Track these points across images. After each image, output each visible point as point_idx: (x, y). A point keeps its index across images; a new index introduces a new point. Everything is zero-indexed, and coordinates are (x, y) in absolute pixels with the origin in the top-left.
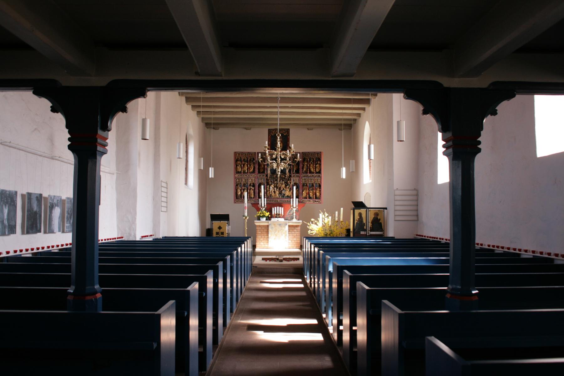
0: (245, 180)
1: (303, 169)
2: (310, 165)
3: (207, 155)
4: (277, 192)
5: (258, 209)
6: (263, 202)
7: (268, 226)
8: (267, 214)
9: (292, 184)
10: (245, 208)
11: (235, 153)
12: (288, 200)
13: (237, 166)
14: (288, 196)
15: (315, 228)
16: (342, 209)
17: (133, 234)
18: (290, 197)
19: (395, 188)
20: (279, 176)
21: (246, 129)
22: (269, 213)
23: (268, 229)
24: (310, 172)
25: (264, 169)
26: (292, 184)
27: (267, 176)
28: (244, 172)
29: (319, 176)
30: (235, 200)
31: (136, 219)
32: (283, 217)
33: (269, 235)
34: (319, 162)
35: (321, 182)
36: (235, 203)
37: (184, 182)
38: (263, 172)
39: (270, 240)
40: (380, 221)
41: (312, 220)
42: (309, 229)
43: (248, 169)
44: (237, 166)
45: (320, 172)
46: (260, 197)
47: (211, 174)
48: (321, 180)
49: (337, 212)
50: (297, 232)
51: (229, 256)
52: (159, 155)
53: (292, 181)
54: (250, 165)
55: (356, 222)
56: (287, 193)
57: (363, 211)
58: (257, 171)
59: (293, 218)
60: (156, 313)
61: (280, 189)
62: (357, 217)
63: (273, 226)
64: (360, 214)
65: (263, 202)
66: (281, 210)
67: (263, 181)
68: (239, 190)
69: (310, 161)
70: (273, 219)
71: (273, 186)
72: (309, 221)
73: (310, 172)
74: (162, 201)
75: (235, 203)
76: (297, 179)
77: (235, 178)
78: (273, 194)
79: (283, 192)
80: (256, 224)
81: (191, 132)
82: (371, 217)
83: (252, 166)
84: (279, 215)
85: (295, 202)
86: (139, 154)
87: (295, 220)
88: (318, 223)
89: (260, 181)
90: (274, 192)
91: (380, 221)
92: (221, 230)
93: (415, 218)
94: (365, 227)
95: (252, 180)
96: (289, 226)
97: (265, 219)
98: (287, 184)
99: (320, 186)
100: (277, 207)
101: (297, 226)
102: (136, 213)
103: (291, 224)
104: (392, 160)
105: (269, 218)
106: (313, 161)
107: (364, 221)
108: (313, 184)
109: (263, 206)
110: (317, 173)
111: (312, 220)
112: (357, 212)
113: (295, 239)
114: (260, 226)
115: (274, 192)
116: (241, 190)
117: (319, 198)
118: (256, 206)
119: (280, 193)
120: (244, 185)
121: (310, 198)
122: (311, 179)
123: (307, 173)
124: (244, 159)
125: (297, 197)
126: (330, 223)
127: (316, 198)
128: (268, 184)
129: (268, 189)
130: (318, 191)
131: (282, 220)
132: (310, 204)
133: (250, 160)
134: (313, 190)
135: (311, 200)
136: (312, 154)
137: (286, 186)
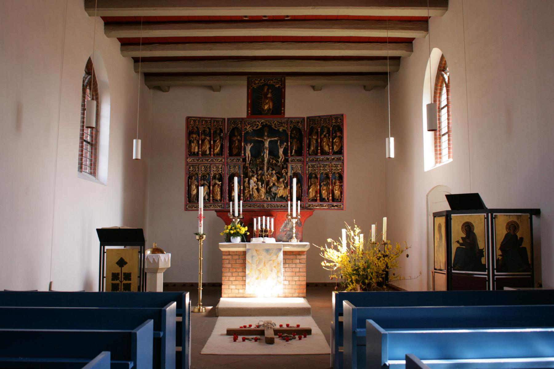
0: (206, 168)
1: (309, 147)
3: (137, 125)
4: (263, 190)
5: (228, 221)
6: (237, 207)
7: (244, 253)
8: (244, 230)
10: (199, 217)
11: (188, 118)
12: (283, 204)
13: (190, 142)
14: (282, 197)
15: (336, 257)
16: (385, 219)
20: (266, 159)
21: (211, 88)
22: (246, 228)
23: (245, 260)
24: (323, 153)
25: (240, 148)
26: (289, 174)
27: (244, 160)
28: (204, 154)
29: (339, 159)
30: (186, 206)
32: (273, 236)
34: (338, 134)
35: (342, 170)
36: (186, 209)
37: (77, 166)
38: (239, 154)
40: (524, 245)
41: (329, 240)
42: (323, 259)
43: (210, 148)
44: (190, 142)
45: (340, 152)
46: (231, 199)
48: (342, 166)
49: (373, 227)
50: (300, 266)
51: (150, 324)
53: (290, 169)
54: (215, 142)
55: (454, 246)
56: (281, 192)
57: (477, 219)
58: (226, 151)
59: (291, 238)
60: (132, 331)
61: (268, 183)
62: (457, 233)
63: (255, 253)
64: (468, 228)
65: (237, 207)
66: (269, 223)
69: (321, 134)
70: (254, 240)
72: (323, 242)
73: (323, 153)
75: (186, 209)
76: (299, 165)
77: (187, 164)
78: (256, 194)
79: (273, 190)
80: (223, 249)
82: (501, 232)
83: (218, 143)
84: (266, 231)
85: (295, 207)
87: (294, 242)
88: (339, 247)
89: (232, 170)
90: (258, 190)
91: (524, 245)
92: (125, 269)
95: (217, 167)
96: (285, 253)
97: (238, 239)
98: (280, 176)
100: (261, 216)
101: (300, 253)
103: (288, 249)
105: (246, 238)
106: (329, 132)
107: (481, 245)
108: (327, 174)
109: (236, 214)
110: (335, 153)
111: (329, 240)
112: (458, 220)
113: (296, 278)
114: (229, 253)
115: (258, 190)
117: (340, 200)
118: (224, 215)
119: (268, 192)
120: (204, 177)
121: (322, 200)
122: (325, 166)
123: (317, 154)
124: (204, 131)
125: (298, 199)
126: (361, 247)
127: (333, 200)
128: (246, 175)
129: (246, 184)
130: (337, 187)
131: (271, 241)
132: (323, 213)
133: (215, 132)
134: (327, 184)
135: (325, 204)
137: (278, 179)
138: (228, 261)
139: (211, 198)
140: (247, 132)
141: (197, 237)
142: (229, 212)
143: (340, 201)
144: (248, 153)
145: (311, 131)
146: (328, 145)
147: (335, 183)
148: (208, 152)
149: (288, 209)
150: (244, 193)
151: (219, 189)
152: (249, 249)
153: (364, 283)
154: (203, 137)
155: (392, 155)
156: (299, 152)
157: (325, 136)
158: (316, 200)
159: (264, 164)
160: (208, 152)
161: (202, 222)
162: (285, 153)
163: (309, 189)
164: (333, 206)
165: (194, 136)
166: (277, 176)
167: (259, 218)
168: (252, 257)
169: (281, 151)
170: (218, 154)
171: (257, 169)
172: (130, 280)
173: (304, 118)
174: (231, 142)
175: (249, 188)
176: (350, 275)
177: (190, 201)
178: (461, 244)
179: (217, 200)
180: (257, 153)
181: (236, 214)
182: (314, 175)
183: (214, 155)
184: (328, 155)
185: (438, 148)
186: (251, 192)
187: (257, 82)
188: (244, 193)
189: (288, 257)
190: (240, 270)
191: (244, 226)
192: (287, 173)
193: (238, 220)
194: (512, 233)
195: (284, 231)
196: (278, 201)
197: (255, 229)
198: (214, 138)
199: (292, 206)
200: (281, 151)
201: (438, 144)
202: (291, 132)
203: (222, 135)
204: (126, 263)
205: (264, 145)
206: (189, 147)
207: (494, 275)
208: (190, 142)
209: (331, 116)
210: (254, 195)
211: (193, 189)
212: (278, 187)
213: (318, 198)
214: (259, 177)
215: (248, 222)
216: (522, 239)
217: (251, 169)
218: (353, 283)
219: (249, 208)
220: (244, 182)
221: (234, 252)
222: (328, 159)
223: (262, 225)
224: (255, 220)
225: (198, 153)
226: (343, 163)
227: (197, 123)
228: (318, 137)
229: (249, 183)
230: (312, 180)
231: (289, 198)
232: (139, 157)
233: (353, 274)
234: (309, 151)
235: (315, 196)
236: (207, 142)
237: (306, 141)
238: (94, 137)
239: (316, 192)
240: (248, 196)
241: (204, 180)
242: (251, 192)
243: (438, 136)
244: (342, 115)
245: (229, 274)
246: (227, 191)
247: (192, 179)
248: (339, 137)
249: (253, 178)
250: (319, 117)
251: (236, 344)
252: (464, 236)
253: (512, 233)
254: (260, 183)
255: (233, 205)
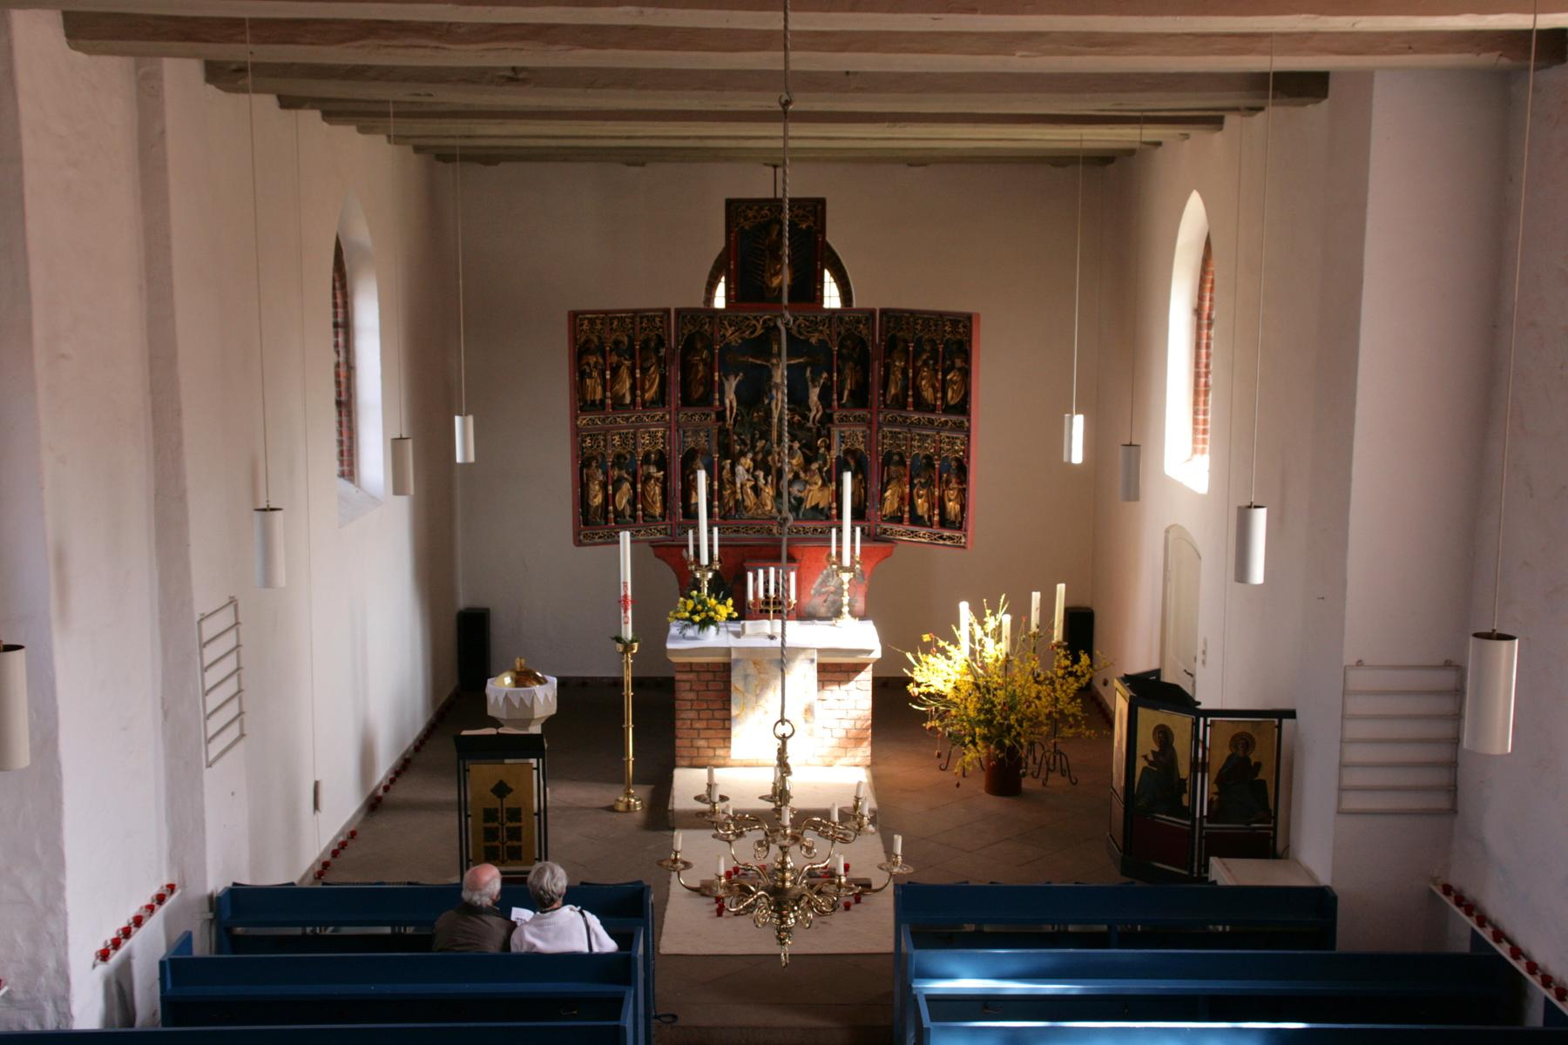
0: (624, 438)
1: (885, 386)
2: (917, 372)
4: (769, 492)
6: (705, 541)
9: (834, 453)
11: (574, 316)
12: (819, 525)
17: (51, 964)
18: (829, 515)
19: (1349, 660)
23: (728, 683)
24: (920, 405)
26: (834, 453)
27: (721, 416)
28: (618, 403)
29: (959, 427)
30: (577, 534)
31: (61, 888)
33: (734, 712)
35: (967, 452)
37: (335, 467)
38: (706, 400)
39: (736, 731)
40: (1261, 776)
41: (926, 638)
42: (911, 680)
43: (633, 389)
45: (963, 408)
46: (691, 515)
47: (463, 449)
49: (1036, 596)
52: (182, 498)
54: (644, 371)
55: (1140, 764)
56: (816, 495)
57: (1179, 723)
58: (675, 395)
62: (1147, 744)
63: (751, 670)
64: (1164, 735)
65: (705, 541)
67: (702, 440)
68: (595, 488)
69: (917, 355)
71: (747, 461)
73: (920, 405)
74: (214, 681)
75: (578, 543)
76: (859, 430)
77: (577, 432)
78: (750, 499)
80: (675, 659)
81: (361, 234)
82: (1219, 756)
84: (777, 602)
85: (848, 540)
86: (61, 559)
90: (756, 490)
91: (1261, 776)
92: (509, 801)
93: (1441, 802)
94: (1185, 800)
95: (653, 436)
99: (962, 470)
102: (59, 863)
104: (1342, 544)
108: (929, 458)
109: (705, 560)
110: (948, 409)
111: (926, 638)
112: (1150, 718)
115: (756, 490)
116: (604, 486)
117: (958, 524)
118: (668, 553)
120: (619, 461)
121: (916, 520)
123: (904, 407)
124: (617, 343)
125: (858, 515)
128: (726, 451)
130: (952, 494)
132: (912, 543)
133: (646, 342)
134: (929, 484)
136: (926, 322)
138: (687, 686)
139: (640, 513)
140: (727, 345)
141: (620, 647)
142: (687, 546)
143: (960, 528)
144: (731, 398)
145: (891, 345)
146: (933, 386)
147: (948, 482)
148: (628, 400)
149: (829, 540)
150: (721, 498)
151: (657, 490)
152: (737, 660)
153: (1000, 745)
154: (615, 359)
155: (1077, 457)
156: (860, 397)
157: (925, 363)
158: (900, 521)
159: (770, 425)
160: (628, 400)
161: (629, 613)
162: (824, 397)
163: (883, 490)
164: (941, 537)
165: (592, 360)
166: (804, 454)
167: (761, 572)
168: (746, 677)
169: (814, 394)
170: (653, 402)
171: (753, 436)
172: (520, 820)
173: (872, 312)
174: (686, 368)
175: (734, 483)
176: (974, 723)
177: (586, 523)
178: (1151, 763)
179: (654, 517)
180: (755, 394)
181: (705, 560)
182: (896, 458)
183: (644, 404)
184: (933, 411)
185: (1201, 417)
186: (739, 496)
187: (750, 214)
188: (721, 498)
189: (829, 676)
190: (718, 705)
191: (722, 602)
192: (828, 448)
193: (710, 575)
194: (1241, 753)
195: (820, 594)
196: (806, 519)
197: (751, 597)
198: (643, 360)
199: (839, 540)
200: (814, 394)
201: (1201, 407)
202: (841, 346)
203: (663, 352)
204: (510, 790)
205: (770, 377)
206: (579, 388)
207: (1202, 828)
208: (580, 374)
209: (941, 315)
210: (748, 503)
211: (592, 493)
212: (806, 482)
213: (906, 516)
214: (760, 456)
215: (729, 584)
216: (1258, 765)
217: (739, 435)
218: (975, 744)
219: (734, 535)
220: (722, 468)
221: (701, 665)
222: (931, 422)
223: (766, 590)
224: (750, 575)
225: (602, 401)
226: (968, 436)
227: (599, 327)
228: (907, 362)
229: (733, 473)
230: (893, 468)
231: (834, 512)
232: (472, 459)
233: (979, 723)
234: (884, 395)
235: (899, 509)
236: (624, 372)
237: (877, 370)
238: (343, 389)
239: (902, 499)
240: (732, 504)
241: (620, 469)
242: (739, 496)
243: (1202, 388)
244: (969, 317)
245: (692, 714)
246: (679, 494)
247: (589, 466)
248: (959, 369)
249: (743, 460)
250: (912, 313)
251: (724, 922)
252: (1156, 749)
253: (1241, 753)
254: (761, 474)
255: (696, 534)
